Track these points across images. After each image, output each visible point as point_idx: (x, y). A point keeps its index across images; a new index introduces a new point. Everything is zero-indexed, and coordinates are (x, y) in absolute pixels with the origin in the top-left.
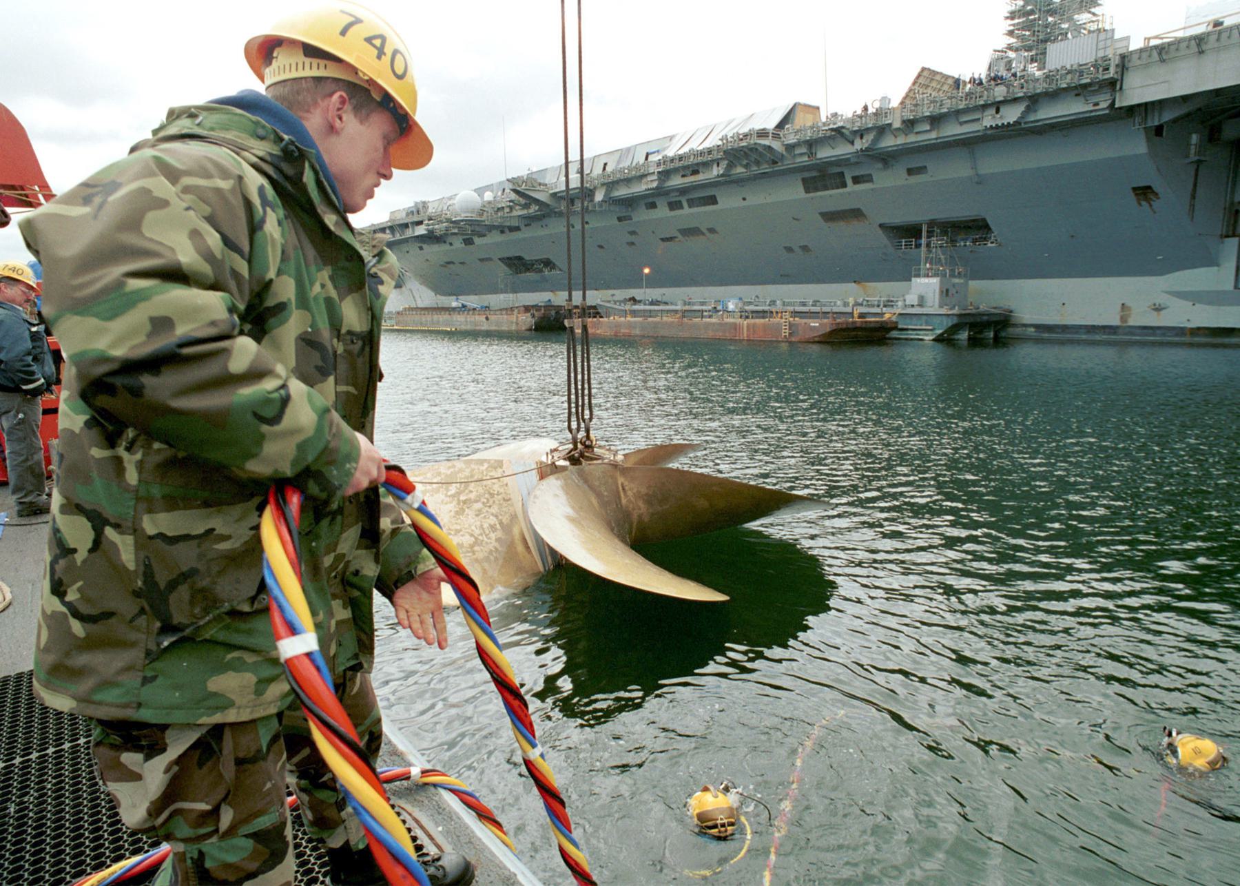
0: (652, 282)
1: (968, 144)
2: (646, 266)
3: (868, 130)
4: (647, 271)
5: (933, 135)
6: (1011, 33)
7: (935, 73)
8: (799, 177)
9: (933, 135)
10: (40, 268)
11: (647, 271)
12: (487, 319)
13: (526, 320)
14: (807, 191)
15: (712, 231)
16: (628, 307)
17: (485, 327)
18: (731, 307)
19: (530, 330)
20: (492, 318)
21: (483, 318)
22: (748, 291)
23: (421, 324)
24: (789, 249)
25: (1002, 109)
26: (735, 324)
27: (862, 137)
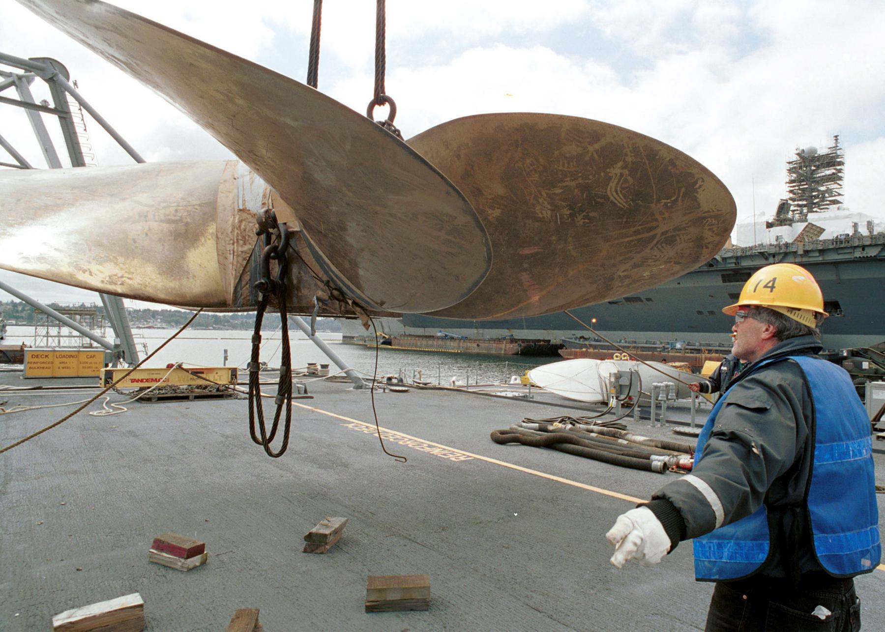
0: (596, 327)
1: (836, 264)
2: (593, 318)
3: (779, 254)
4: (594, 321)
5: (820, 259)
6: (791, 191)
7: (813, 225)
8: (720, 274)
9: (820, 259)
10: (389, 326)
11: (594, 321)
12: (478, 345)
13: (514, 348)
14: (724, 281)
15: (649, 300)
16: (582, 342)
17: (476, 350)
18: (678, 346)
19: (517, 354)
20: (482, 345)
21: (475, 345)
22: (688, 336)
23: (416, 346)
24: (700, 313)
25: (866, 249)
26: (696, 358)
27: (774, 257)
